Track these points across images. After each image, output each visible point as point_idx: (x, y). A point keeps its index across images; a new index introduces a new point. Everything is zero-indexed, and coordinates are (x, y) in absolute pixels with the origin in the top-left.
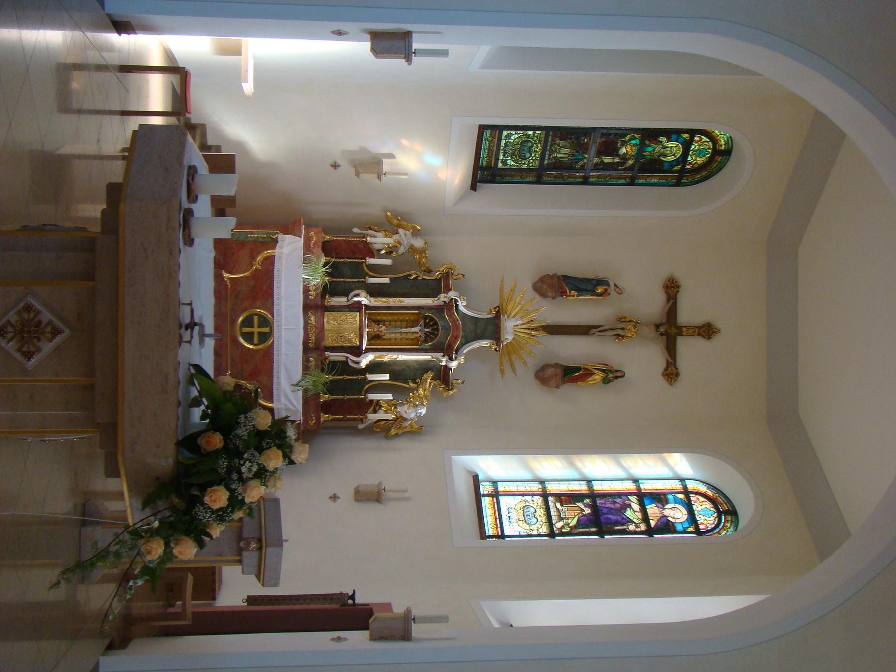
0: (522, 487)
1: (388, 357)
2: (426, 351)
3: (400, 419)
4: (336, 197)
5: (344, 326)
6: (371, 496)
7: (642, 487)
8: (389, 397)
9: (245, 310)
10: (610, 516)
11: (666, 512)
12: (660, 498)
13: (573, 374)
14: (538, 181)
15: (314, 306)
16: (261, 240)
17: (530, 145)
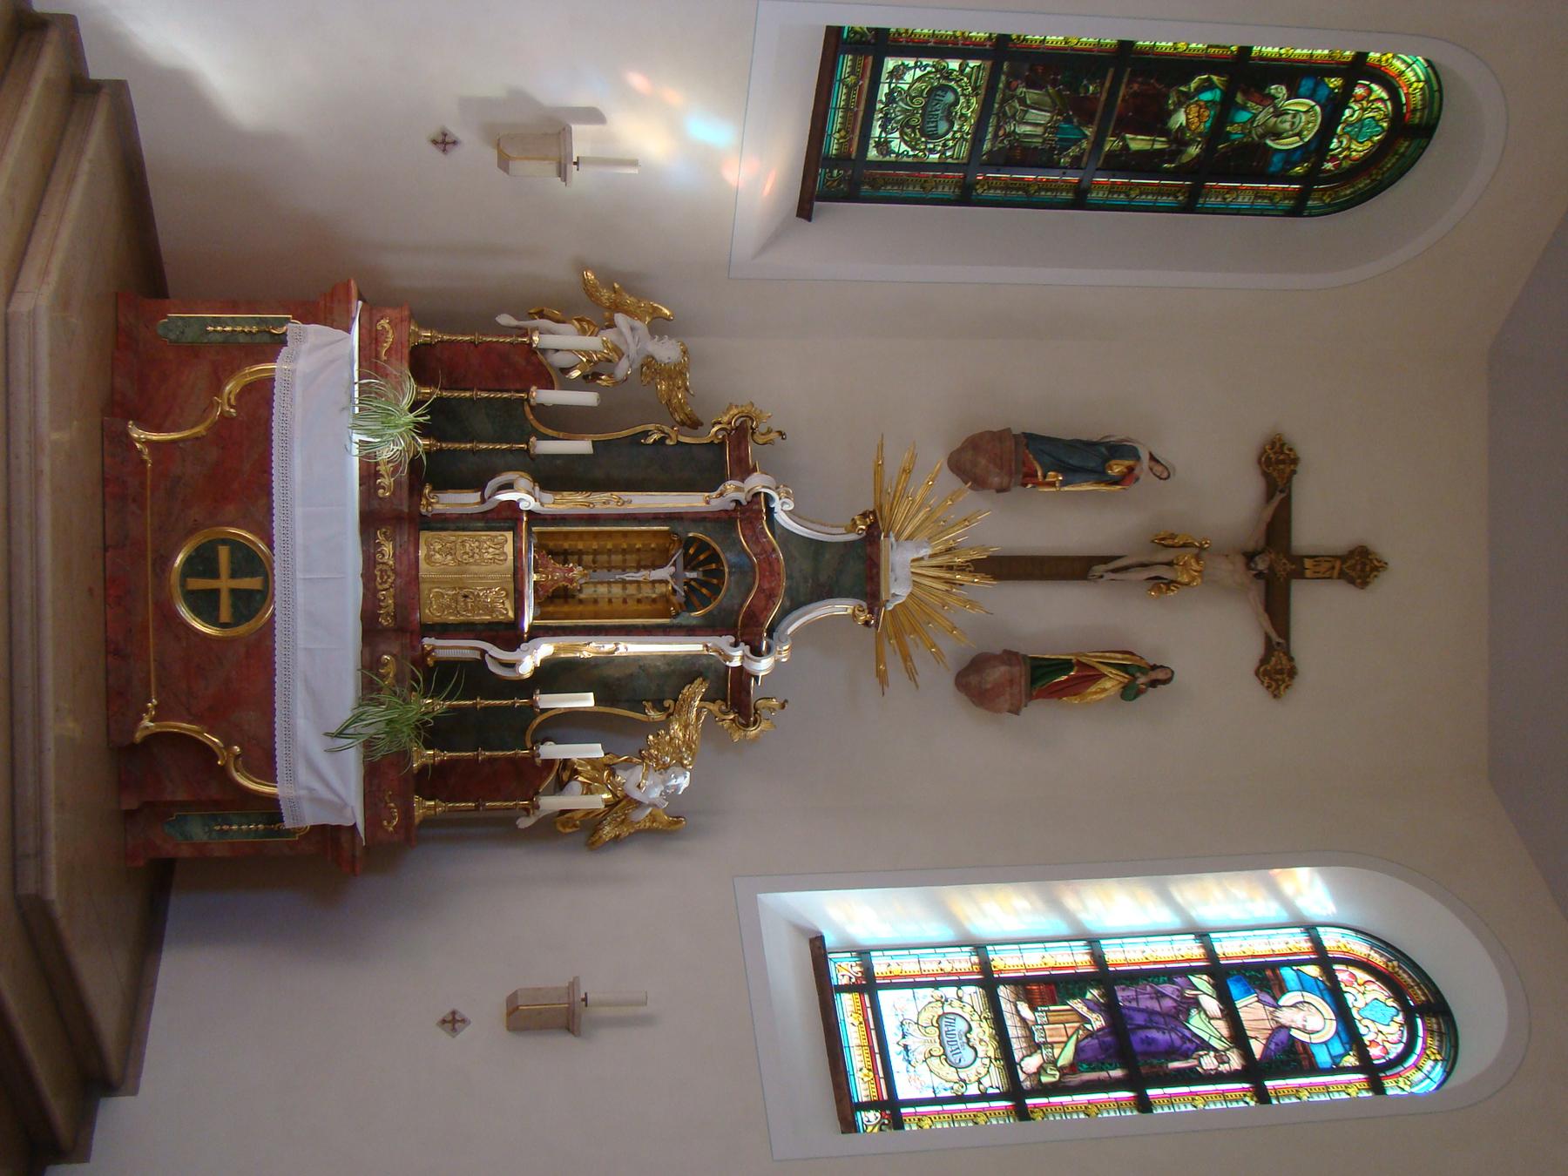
0: (931, 963)
1: (591, 648)
2: (690, 631)
3: (622, 803)
4: (452, 229)
5: (473, 567)
6: (552, 1017)
7: (1219, 950)
8: (596, 751)
9: (192, 532)
10: (1154, 1034)
11: (1285, 1017)
12: (1264, 977)
13: (1050, 677)
14: (966, 196)
15: (391, 514)
16: (242, 339)
17: (950, 97)
